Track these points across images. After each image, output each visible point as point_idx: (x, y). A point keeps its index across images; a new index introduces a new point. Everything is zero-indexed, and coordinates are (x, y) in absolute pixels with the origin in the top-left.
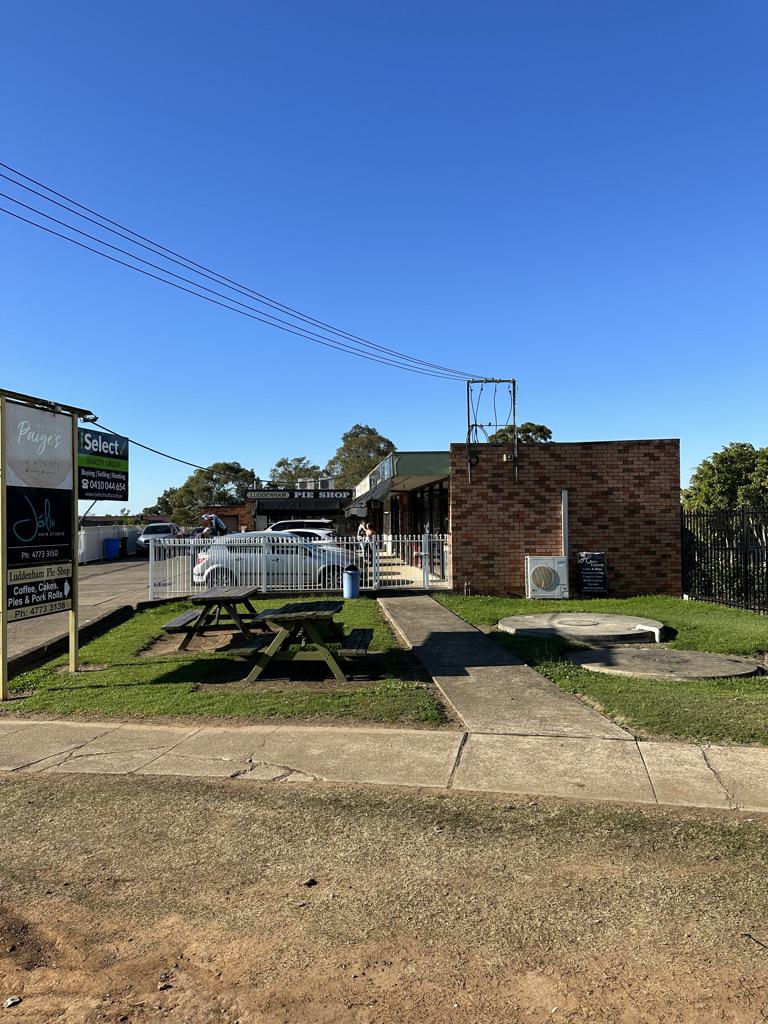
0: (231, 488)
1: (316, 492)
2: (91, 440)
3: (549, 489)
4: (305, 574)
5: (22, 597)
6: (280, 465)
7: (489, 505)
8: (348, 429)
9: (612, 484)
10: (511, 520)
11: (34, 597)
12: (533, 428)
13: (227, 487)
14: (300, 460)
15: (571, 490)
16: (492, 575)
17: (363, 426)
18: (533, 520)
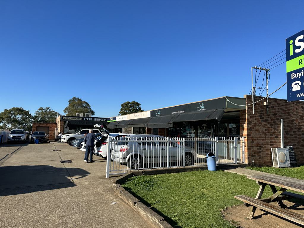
0: (19, 117)
1: (83, 118)
3: (277, 119)
4: (176, 157)
6: (40, 109)
7: (259, 124)
8: (71, 98)
9: (294, 118)
10: (266, 132)
12: (135, 103)
13: (17, 117)
14: (48, 108)
15: (284, 119)
16: (260, 157)
17: (77, 98)
18: (272, 132)
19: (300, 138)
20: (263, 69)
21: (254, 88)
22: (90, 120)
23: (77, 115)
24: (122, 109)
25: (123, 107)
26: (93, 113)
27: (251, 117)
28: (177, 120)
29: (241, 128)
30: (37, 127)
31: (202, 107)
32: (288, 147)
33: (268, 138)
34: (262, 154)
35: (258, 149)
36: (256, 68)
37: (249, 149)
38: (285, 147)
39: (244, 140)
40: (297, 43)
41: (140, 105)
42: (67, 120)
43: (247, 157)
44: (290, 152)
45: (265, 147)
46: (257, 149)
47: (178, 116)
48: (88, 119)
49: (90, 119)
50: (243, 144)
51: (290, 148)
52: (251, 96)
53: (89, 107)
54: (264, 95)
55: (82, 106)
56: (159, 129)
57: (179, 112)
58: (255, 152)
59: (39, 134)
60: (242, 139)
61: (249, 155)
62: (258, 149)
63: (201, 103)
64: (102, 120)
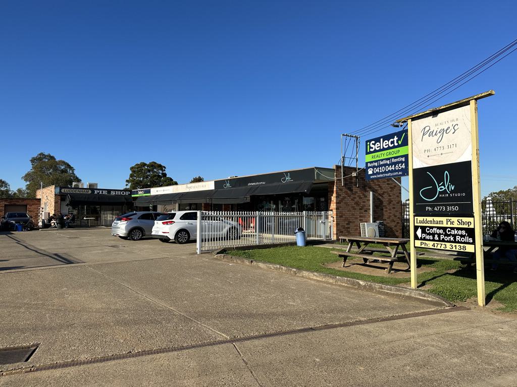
2: (374, 144)
5: (433, 235)
8: (35, 155)
11: (442, 237)
17: (46, 154)
19: (390, 213)
20: (353, 137)
21: (344, 157)
22: (104, 193)
23: (75, 185)
24: (131, 176)
25: (134, 172)
26: (79, 181)
27: (339, 189)
28: (257, 193)
29: (329, 201)
30: (5, 205)
31: (288, 178)
32: (378, 222)
33: (357, 213)
34: (350, 230)
35: (347, 224)
36: (346, 135)
37: (337, 224)
38: (374, 221)
39: (332, 213)
40: (372, 146)
41: (165, 168)
42: (67, 194)
43: (335, 232)
44: (379, 227)
45: (354, 222)
46: (345, 224)
47: (257, 187)
48: (101, 191)
49: (104, 191)
50: (332, 219)
51: (380, 223)
52: (340, 167)
53: (71, 172)
54: (353, 165)
55: (56, 169)
56: (225, 205)
57: (257, 183)
58: (344, 227)
59: (18, 217)
60: (330, 213)
61: (337, 230)
62: (347, 224)
63: (287, 173)
64: (123, 193)
